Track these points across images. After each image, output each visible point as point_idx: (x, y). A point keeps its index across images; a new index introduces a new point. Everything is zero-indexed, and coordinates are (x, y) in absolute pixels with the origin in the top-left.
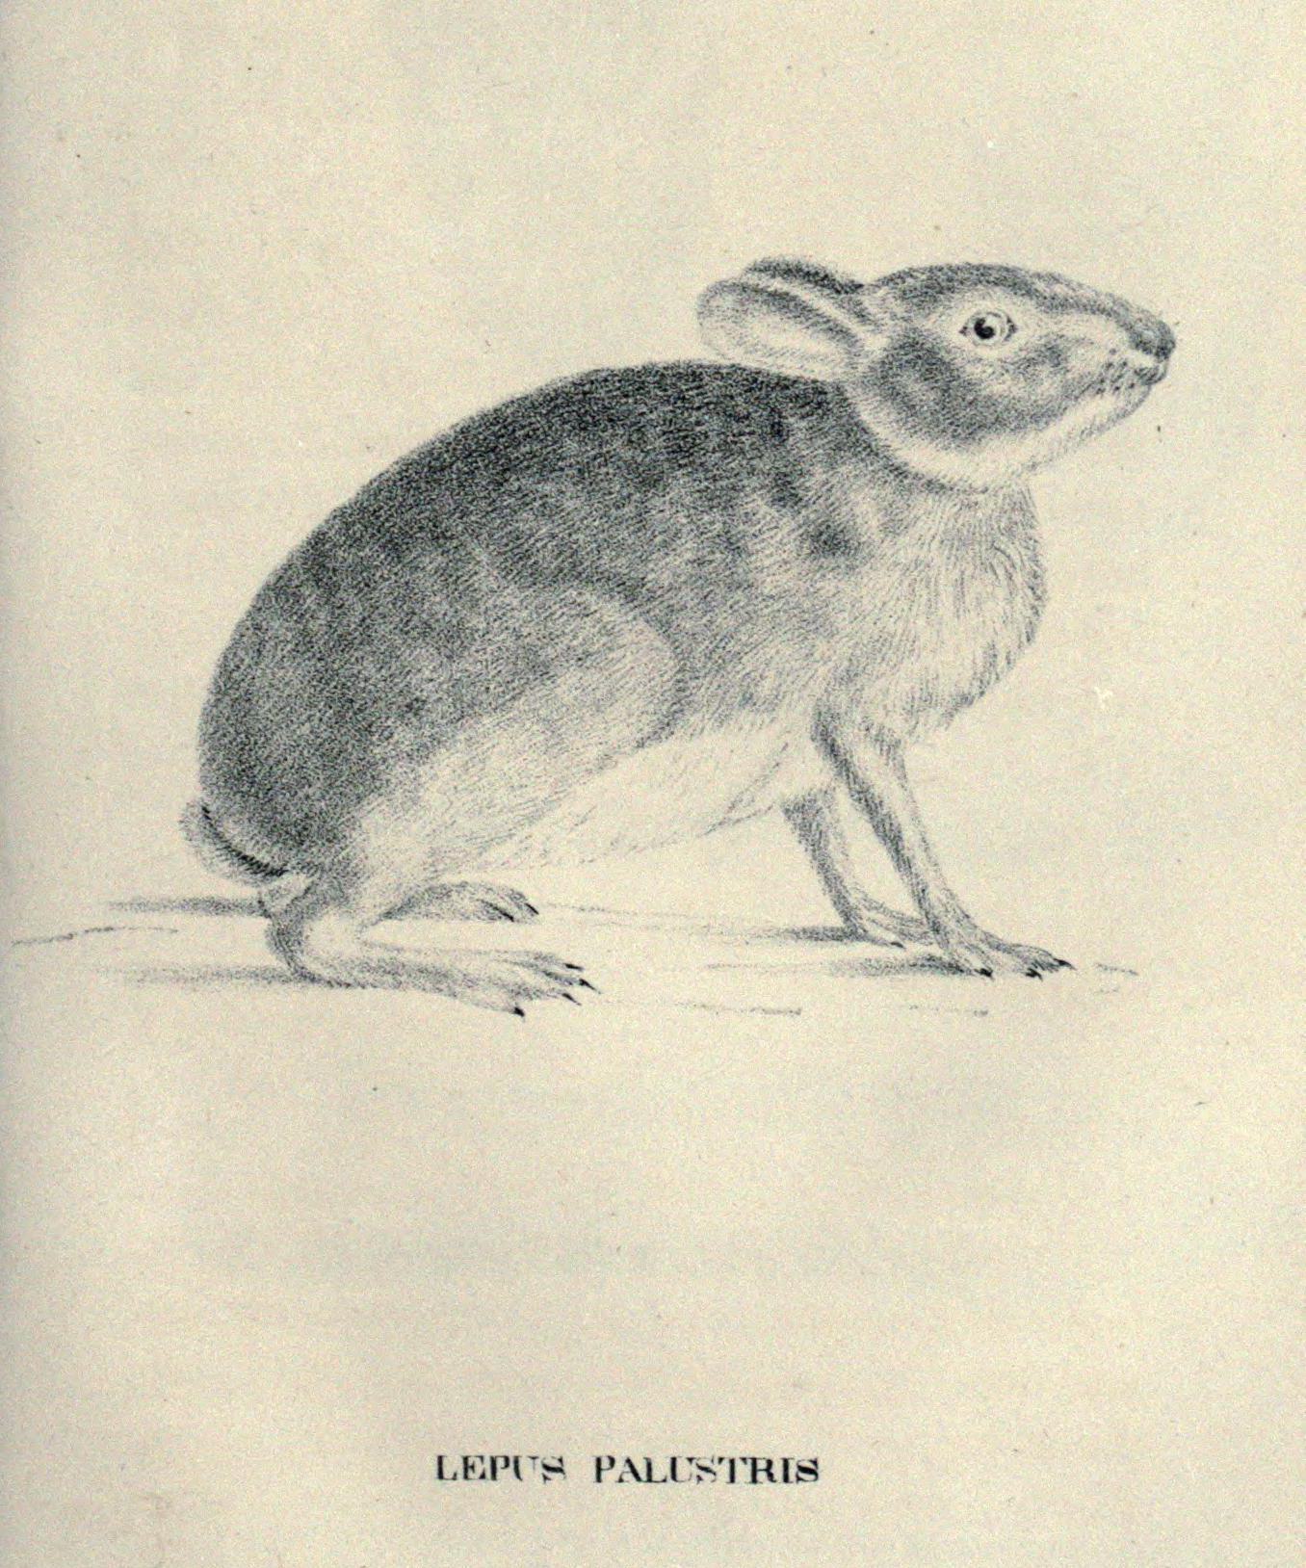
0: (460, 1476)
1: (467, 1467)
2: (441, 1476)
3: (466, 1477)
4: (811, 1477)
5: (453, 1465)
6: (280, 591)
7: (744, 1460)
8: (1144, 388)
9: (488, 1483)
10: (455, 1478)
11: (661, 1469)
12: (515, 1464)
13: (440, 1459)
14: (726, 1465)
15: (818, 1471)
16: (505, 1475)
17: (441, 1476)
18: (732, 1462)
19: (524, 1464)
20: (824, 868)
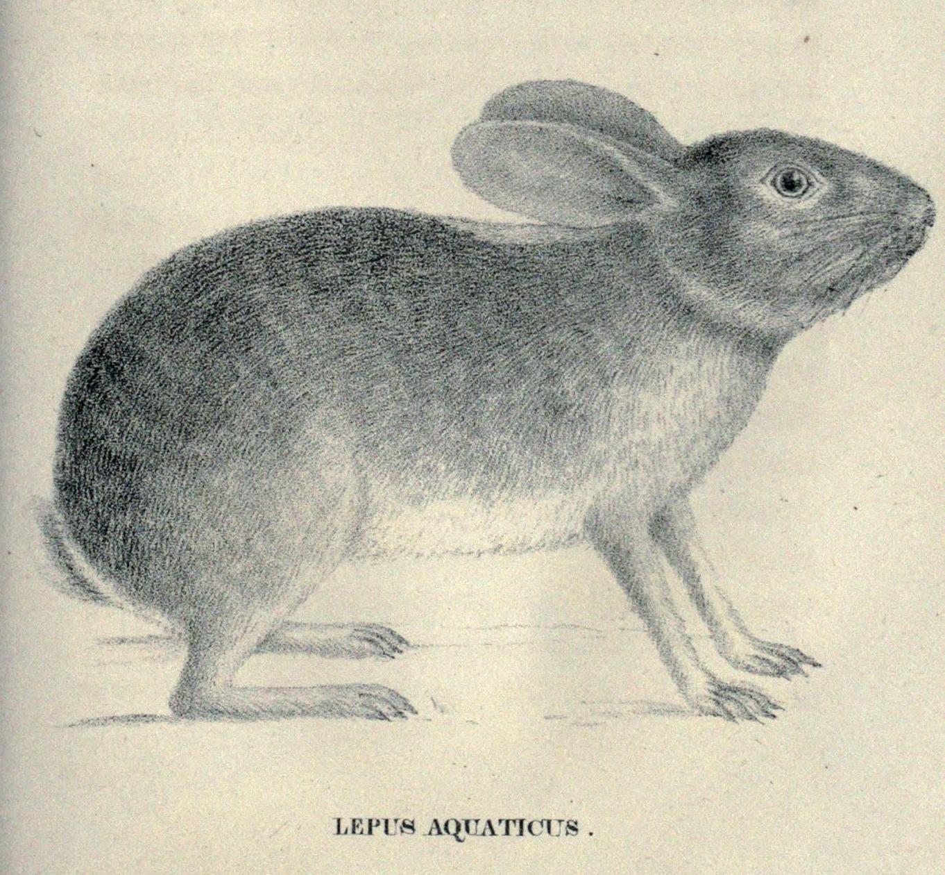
0: (350, 831)
1: (354, 827)
2: (339, 832)
3: (354, 832)
4: (410, 831)
5: (347, 824)
6: (918, 246)
7: (514, 821)
8: (843, 311)
9: (366, 837)
10: (346, 832)
11: (514, 829)
12: (439, 828)
13: (339, 820)
14: (503, 824)
15: (415, 827)
16: (379, 831)
17: (339, 832)
18: (507, 822)
19: (554, 825)
20: (236, 714)
